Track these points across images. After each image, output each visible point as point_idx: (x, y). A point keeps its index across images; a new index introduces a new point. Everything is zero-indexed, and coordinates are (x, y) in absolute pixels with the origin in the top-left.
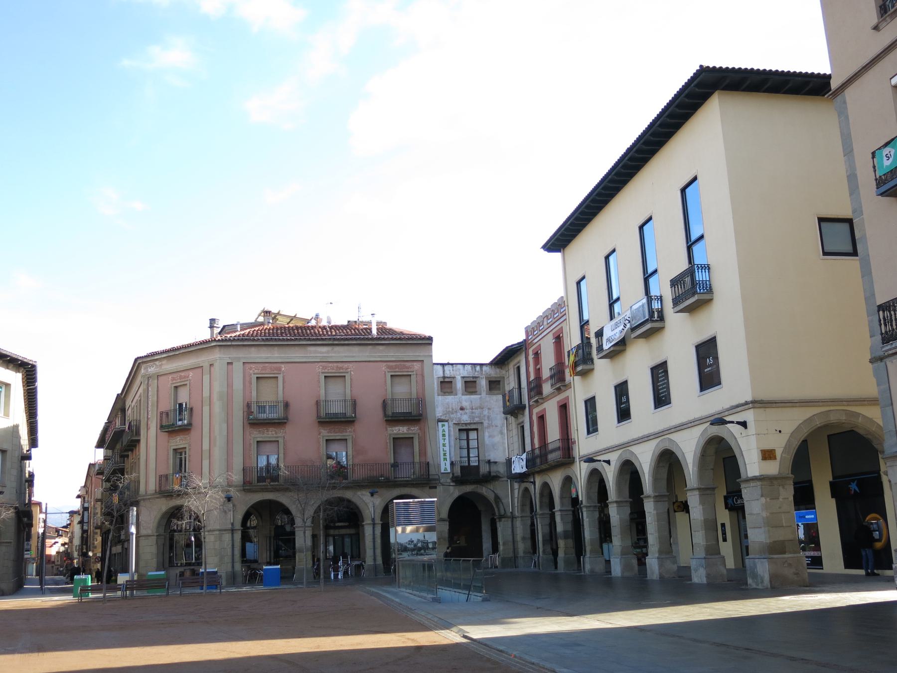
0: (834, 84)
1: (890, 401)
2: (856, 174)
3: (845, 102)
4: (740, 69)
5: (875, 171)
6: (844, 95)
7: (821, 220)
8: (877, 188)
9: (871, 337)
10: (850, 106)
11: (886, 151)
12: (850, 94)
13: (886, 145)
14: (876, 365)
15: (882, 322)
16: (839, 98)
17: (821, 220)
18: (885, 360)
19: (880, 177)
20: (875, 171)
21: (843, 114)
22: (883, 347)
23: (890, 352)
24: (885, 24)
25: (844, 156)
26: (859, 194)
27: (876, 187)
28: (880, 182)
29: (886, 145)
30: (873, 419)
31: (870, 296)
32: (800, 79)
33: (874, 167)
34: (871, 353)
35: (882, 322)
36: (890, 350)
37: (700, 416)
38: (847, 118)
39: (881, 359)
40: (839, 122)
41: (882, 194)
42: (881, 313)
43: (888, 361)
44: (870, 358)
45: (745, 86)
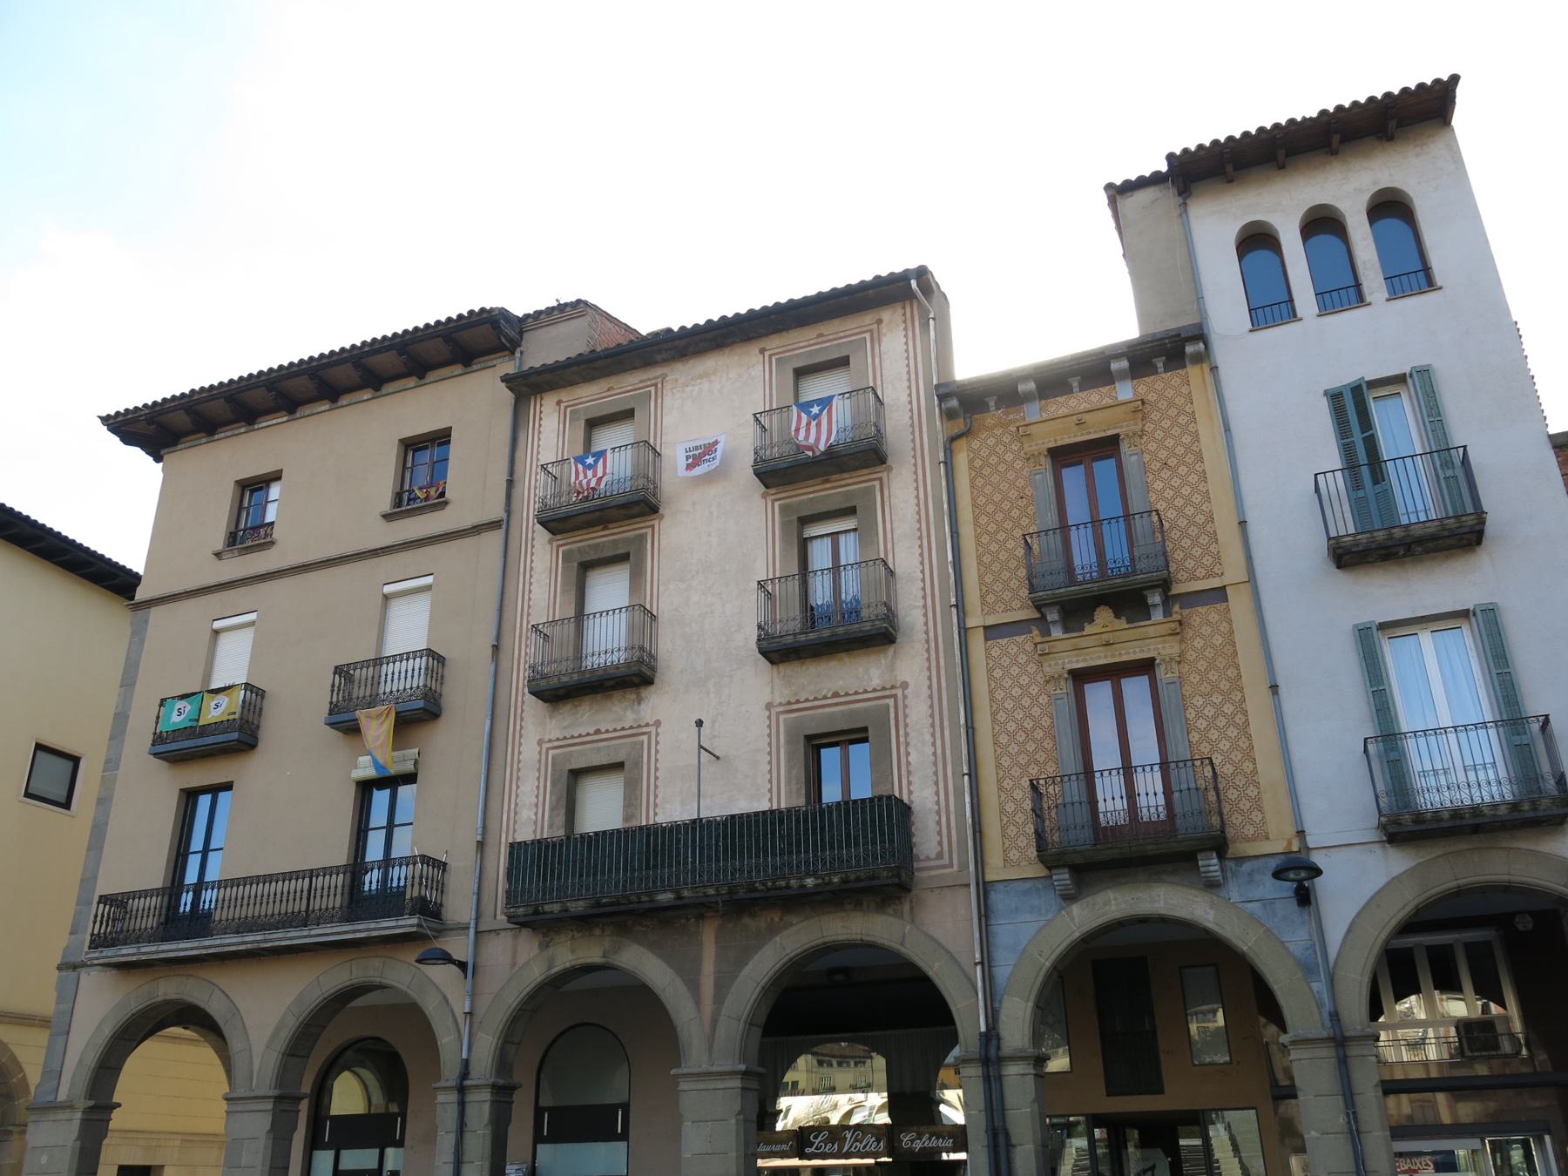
0: (141, 594)
1: (67, 1028)
2: (129, 716)
3: (146, 621)
4: (12, 509)
5: (157, 723)
6: (149, 612)
7: (40, 747)
8: (153, 745)
9: (71, 934)
10: (151, 632)
11: (180, 704)
12: (156, 614)
13: (184, 697)
14: (63, 973)
15: (99, 919)
16: (140, 613)
17: (40, 747)
18: (80, 969)
19: (161, 732)
20: (157, 723)
21: (138, 634)
22: (87, 953)
23: (96, 962)
24: (230, 555)
25: (121, 687)
26: (123, 740)
27: (151, 742)
28: (158, 739)
29: (184, 697)
30: (10, 1046)
31: (88, 881)
32: (84, 555)
33: (158, 717)
34: (63, 957)
35: (99, 919)
36: (97, 958)
37: (986, 1149)
38: (142, 642)
39: (75, 967)
40: (130, 642)
41: (156, 755)
42: (101, 906)
43: (83, 973)
44: (59, 963)
45: (55, 560)
